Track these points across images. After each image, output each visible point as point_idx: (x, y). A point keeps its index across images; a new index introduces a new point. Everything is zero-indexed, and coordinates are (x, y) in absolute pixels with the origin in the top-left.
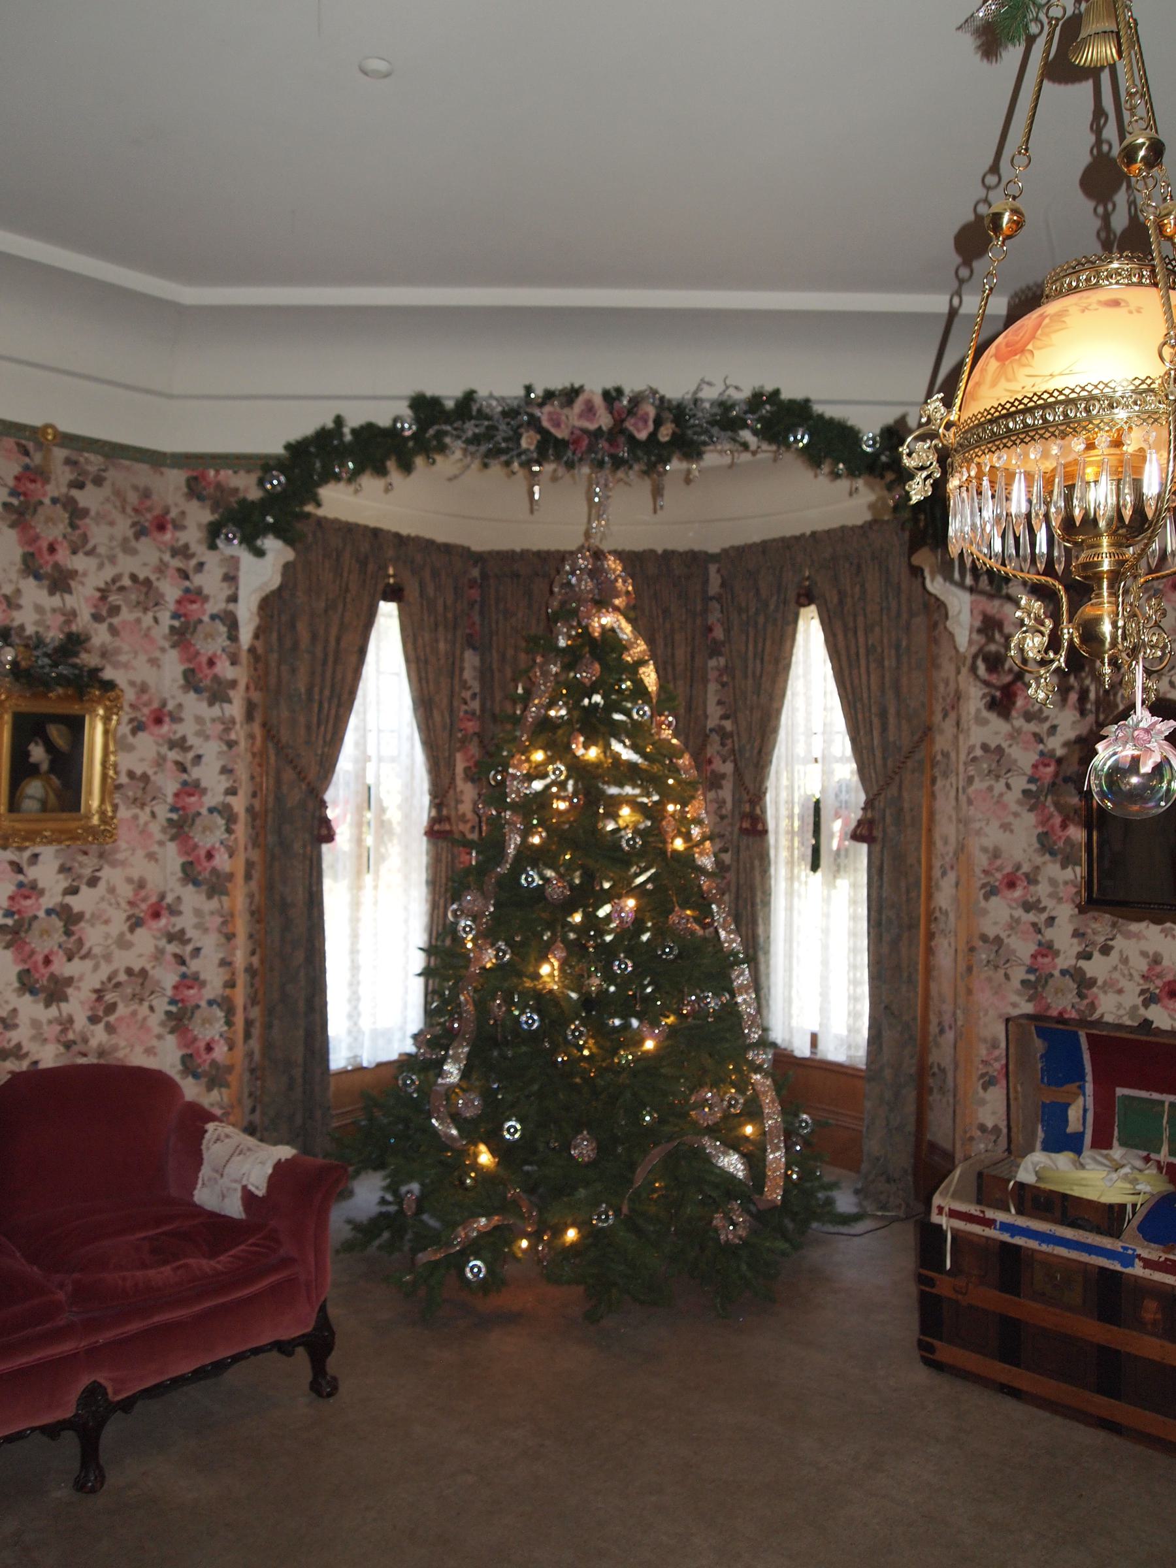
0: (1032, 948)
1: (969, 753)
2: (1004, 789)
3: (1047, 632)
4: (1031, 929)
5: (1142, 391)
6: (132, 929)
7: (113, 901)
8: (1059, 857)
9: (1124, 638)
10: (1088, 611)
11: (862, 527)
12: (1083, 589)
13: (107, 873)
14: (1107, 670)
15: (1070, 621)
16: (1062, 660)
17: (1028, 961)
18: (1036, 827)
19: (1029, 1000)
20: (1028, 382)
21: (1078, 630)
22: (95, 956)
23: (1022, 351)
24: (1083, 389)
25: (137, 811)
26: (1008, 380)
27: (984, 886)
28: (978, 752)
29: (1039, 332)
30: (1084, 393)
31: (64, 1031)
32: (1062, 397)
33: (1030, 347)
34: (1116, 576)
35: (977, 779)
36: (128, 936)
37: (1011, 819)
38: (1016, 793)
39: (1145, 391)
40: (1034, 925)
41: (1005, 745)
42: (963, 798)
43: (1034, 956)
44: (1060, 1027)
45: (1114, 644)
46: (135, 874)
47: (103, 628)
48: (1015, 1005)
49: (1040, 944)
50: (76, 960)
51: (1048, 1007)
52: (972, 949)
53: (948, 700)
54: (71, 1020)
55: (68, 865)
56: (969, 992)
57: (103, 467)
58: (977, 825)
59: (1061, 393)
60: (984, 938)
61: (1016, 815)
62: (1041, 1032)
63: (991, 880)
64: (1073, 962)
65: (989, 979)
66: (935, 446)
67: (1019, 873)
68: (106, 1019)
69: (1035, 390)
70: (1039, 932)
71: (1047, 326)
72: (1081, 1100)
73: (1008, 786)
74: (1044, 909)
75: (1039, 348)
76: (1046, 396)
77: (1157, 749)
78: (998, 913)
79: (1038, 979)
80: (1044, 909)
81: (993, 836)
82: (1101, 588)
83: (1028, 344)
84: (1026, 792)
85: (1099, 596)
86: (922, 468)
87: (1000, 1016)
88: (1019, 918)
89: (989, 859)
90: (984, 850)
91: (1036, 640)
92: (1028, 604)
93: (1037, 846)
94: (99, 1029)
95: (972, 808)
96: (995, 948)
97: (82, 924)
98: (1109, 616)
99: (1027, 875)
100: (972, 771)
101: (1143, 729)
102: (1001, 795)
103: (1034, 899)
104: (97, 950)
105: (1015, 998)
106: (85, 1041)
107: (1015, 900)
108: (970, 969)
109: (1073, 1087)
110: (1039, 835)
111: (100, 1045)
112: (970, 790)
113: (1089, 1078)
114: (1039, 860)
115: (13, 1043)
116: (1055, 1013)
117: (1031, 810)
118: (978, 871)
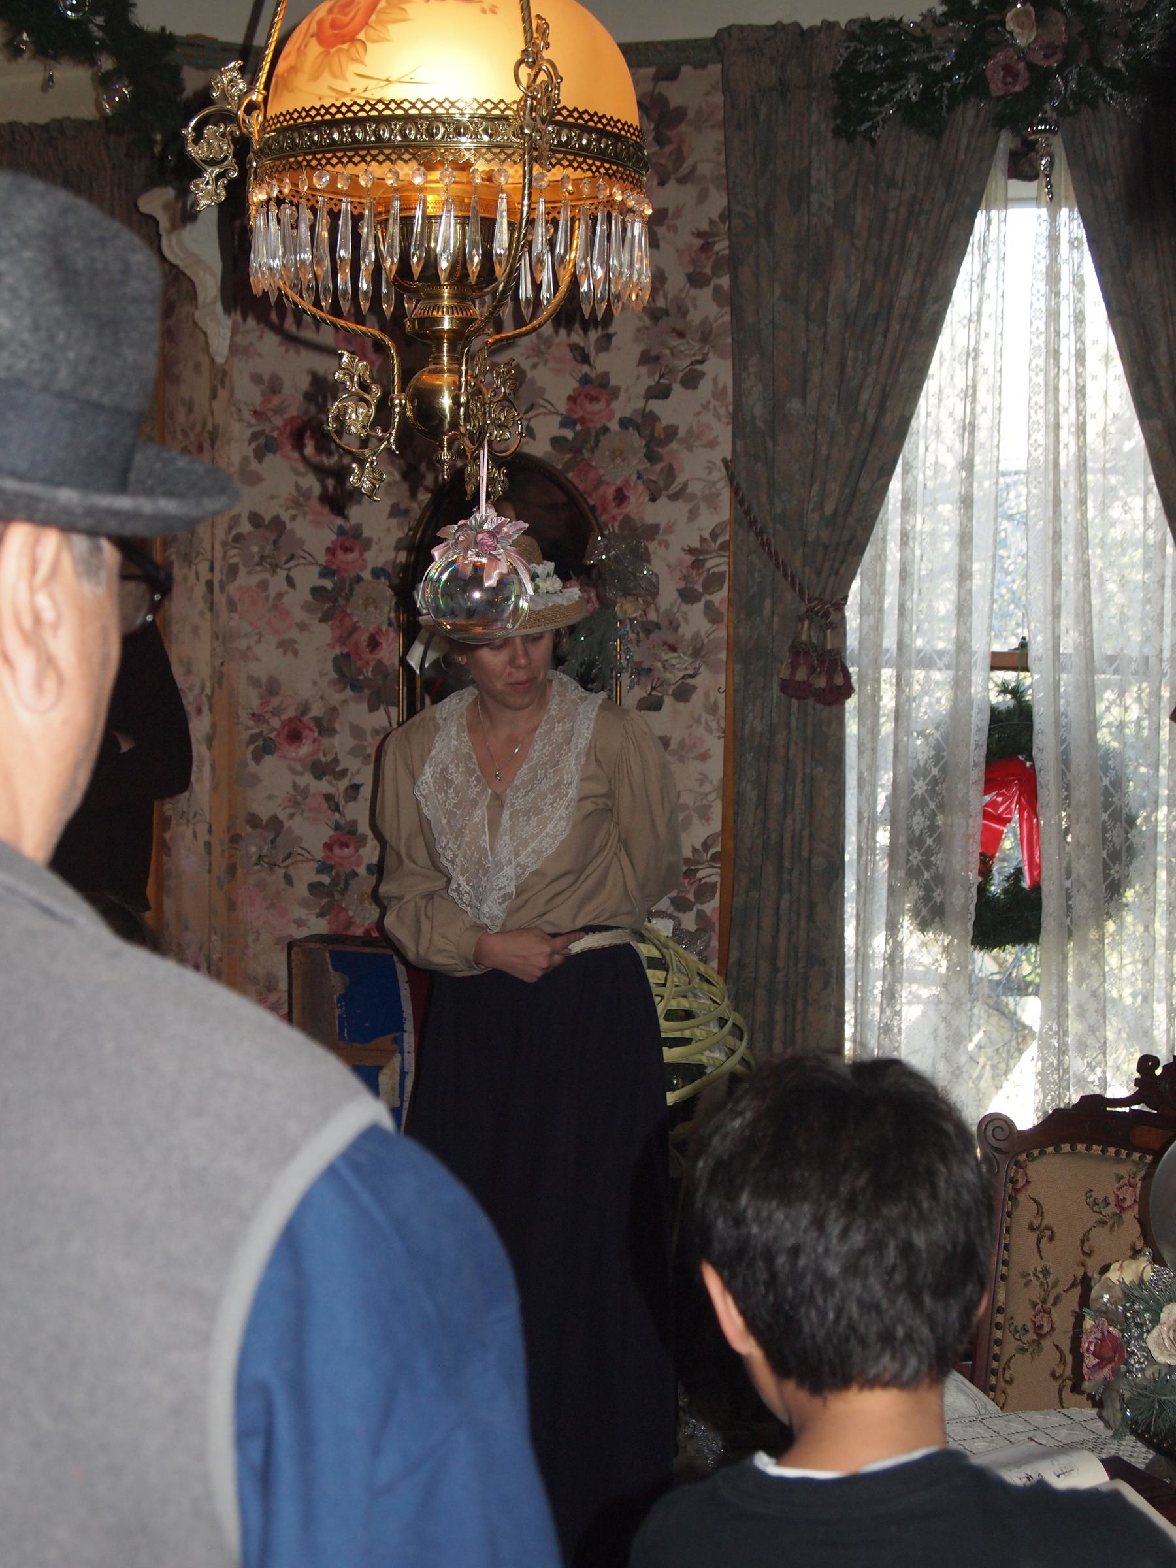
0: (327, 833)
1: (231, 528)
2: (284, 586)
3: (373, 402)
4: (325, 805)
5: (491, 120)
8: (367, 692)
9: (467, 419)
10: (425, 377)
11: (45, 128)
12: (419, 344)
14: (446, 456)
15: (402, 390)
16: (392, 440)
17: (319, 854)
18: (331, 646)
19: (321, 915)
20: (360, 84)
21: (412, 402)
23: (352, 39)
24: (426, 105)
26: (334, 75)
27: (253, 739)
28: (245, 527)
29: (373, 17)
30: (426, 111)
32: (399, 112)
33: (361, 36)
34: (460, 337)
35: (242, 571)
37: (294, 633)
38: (303, 594)
39: (497, 118)
40: (329, 798)
41: (285, 517)
42: (220, 599)
43: (328, 847)
44: (368, 950)
45: (455, 425)
48: (300, 923)
49: (337, 827)
51: (350, 923)
52: (235, 839)
53: (192, 437)
55: (654, 353)
56: (232, 906)
57: (699, 358)
58: (243, 644)
59: (399, 106)
60: (253, 821)
61: (303, 627)
62: (341, 962)
63: (264, 728)
64: (640, 404)
65: (262, 885)
66: (231, 133)
67: (306, 719)
68: (708, 597)
69: (367, 95)
70: (337, 808)
71: (383, 11)
72: (396, 1061)
73: (290, 582)
74: (344, 773)
75: (374, 41)
76: (380, 106)
77: (503, 558)
78: (276, 780)
79: (335, 881)
80: (344, 773)
81: (268, 660)
82: (440, 351)
83: (358, 32)
84: (316, 591)
85: (438, 360)
86: (213, 162)
87: (278, 941)
88: (307, 787)
89: (262, 697)
90: (254, 682)
91: (360, 410)
92: (351, 363)
93: (333, 675)
95: (235, 616)
96: (272, 836)
98: (449, 388)
99: (317, 721)
100: (234, 556)
101: (488, 532)
102: (280, 595)
103: (329, 758)
104: (695, 488)
105: (300, 912)
106: (683, 312)
107: (300, 760)
108: (232, 870)
109: (385, 1041)
110: (336, 660)
111: (696, 636)
112: (231, 588)
113: (409, 1025)
114: (336, 698)
116: (359, 932)
117: (323, 620)
118: (244, 715)
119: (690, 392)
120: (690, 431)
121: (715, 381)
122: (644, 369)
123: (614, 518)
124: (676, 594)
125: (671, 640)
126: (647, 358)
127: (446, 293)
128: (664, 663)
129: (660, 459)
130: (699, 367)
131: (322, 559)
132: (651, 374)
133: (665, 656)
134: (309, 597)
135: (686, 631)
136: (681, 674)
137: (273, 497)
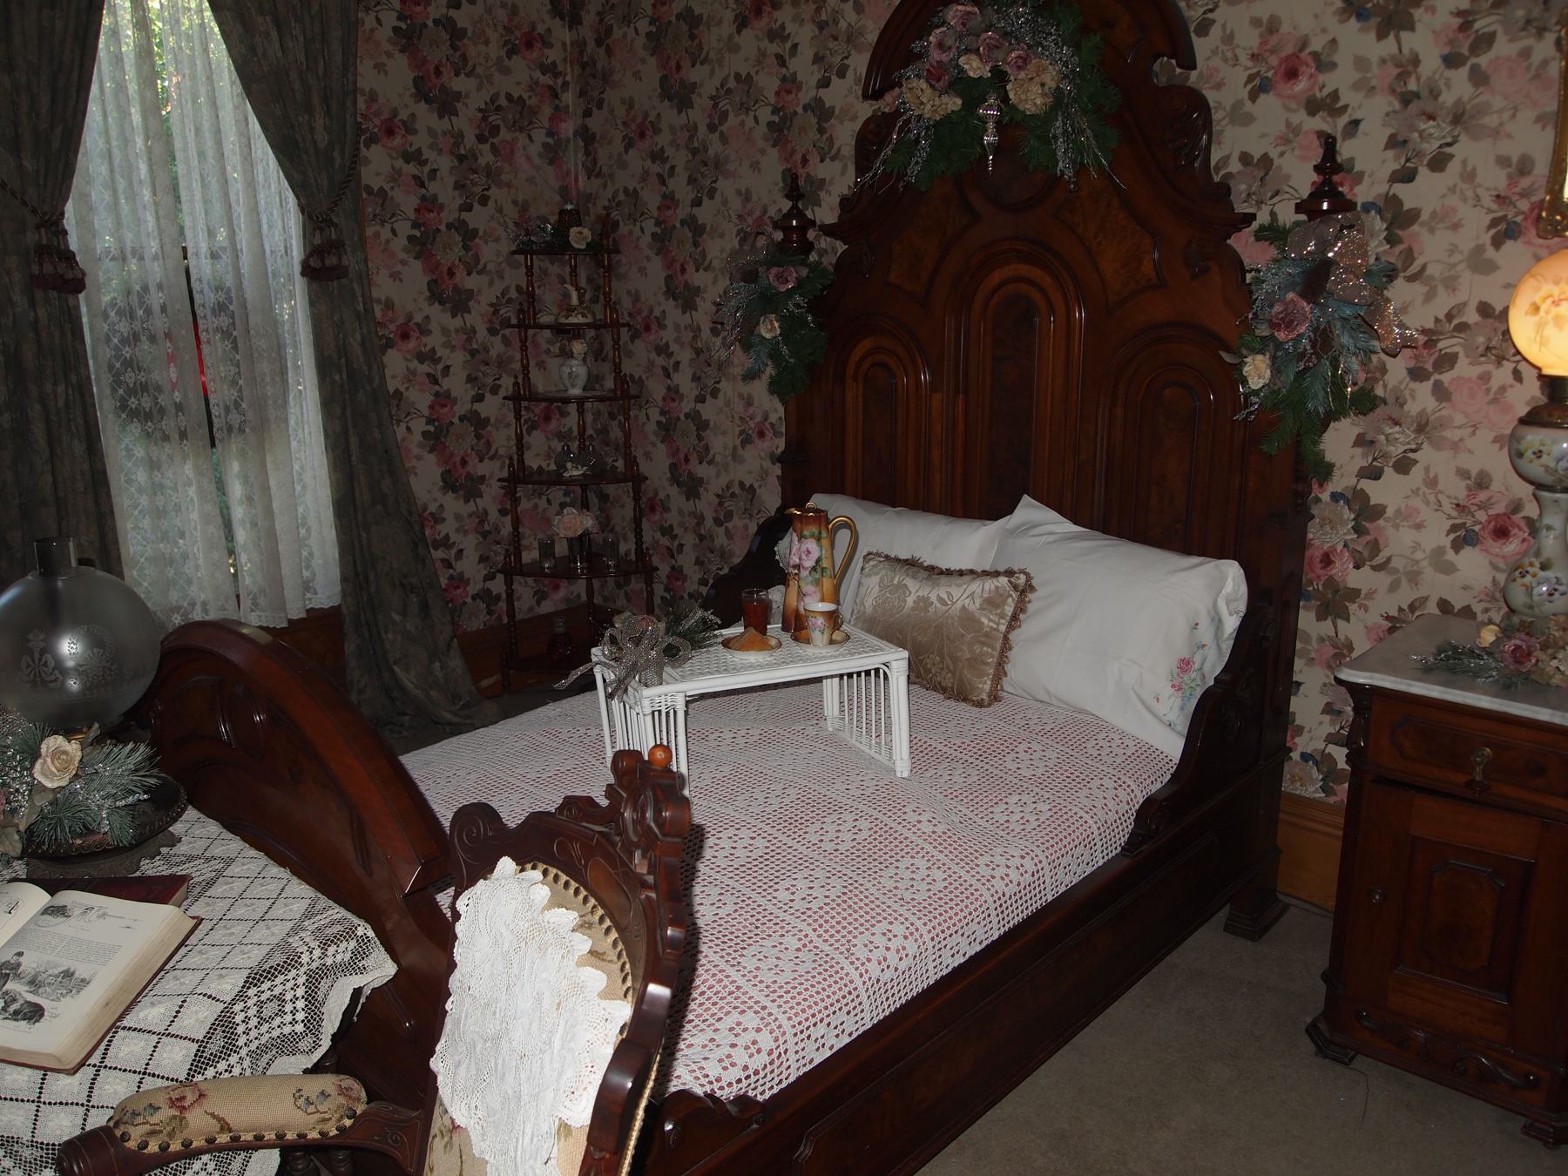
6: (1497, 242)
31: (1403, 76)
36: (1490, 252)
46: (1513, 150)
50: (1366, 569)
54: (1416, 61)
55: (1369, 437)
57: (1449, 140)
68: (1474, 60)
94: (1460, 76)
97: (1415, 228)
104: (1434, 270)
106: (1435, 94)
111: (1459, 102)
115: (1326, 92)
119: (1437, 174)
120: (1434, 214)
122: (1390, 153)
123: (1319, 577)
124: (1439, 61)
125: (1429, 109)
128: (1387, 436)
129: (1400, 241)
130: (1448, 150)
132: (1365, 456)
133: (1422, 126)
135: (1412, 408)
136: (1438, 144)
137: (378, 174)
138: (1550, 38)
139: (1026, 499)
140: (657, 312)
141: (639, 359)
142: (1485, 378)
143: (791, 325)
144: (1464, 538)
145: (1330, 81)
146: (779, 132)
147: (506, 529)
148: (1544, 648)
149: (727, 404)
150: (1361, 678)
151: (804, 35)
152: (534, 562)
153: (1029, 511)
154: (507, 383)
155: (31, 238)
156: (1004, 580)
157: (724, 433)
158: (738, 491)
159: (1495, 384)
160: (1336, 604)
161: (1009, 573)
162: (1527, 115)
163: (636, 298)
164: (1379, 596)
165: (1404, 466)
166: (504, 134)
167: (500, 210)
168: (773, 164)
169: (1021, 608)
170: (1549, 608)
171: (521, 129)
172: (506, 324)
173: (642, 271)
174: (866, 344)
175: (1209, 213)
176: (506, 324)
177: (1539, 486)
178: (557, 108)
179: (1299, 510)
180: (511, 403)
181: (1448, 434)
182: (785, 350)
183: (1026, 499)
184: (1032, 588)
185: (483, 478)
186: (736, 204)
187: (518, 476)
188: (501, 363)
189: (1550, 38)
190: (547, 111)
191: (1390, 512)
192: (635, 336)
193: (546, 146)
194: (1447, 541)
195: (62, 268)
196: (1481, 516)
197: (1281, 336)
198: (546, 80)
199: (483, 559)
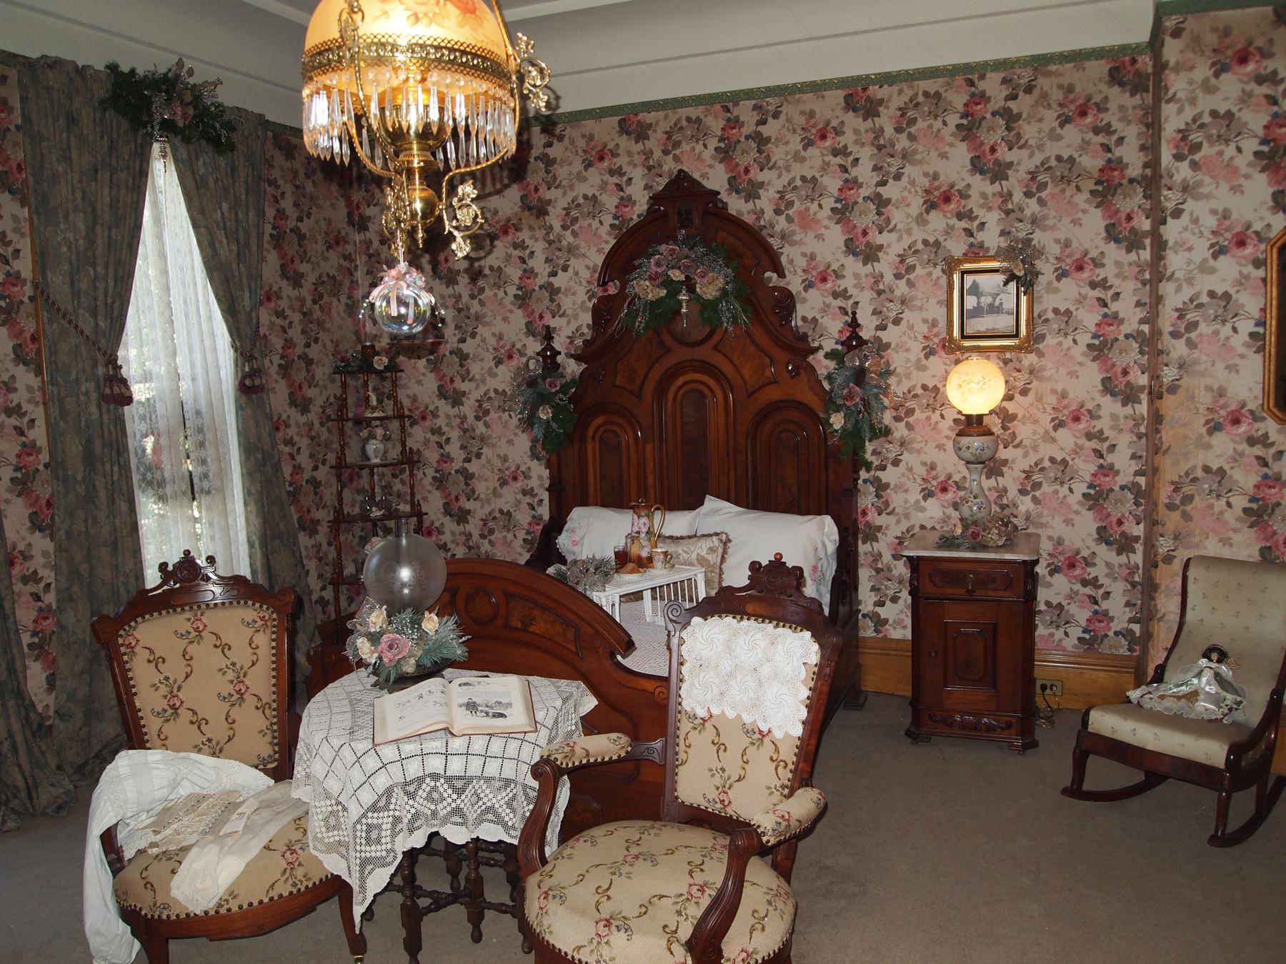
7: (1196, 230)
13: (573, 262)
22: (1026, 446)
25: (1058, 487)
46: (929, 316)
47: (481, 424)
88: (1252, 91)
102: (1069, 349)
107: (1247, 74)
121: (1191, 214)
126: (548, 260)
127: (415, 147)
131: (14, 461)
134: (1247, 339)
138: (939, 268)
139: (708, 497)
140: (284, 417)
141: (417, 437)
142: (928, 418)
143: (557, 409)
144: (928, 494)
145: (843, 284)
146: (523, 299)
147: (333, 554)
148: (984, 530)
149: (489, 461)
150: (912, 554)
151: (539, 247)
152: (352, 575)
153: (711, 503)
154: (331, 458)
155: (101, 371)
156: (715, 538)
157: (486, 480)
158: (498, 515)
159: (933, 421)
160: (872, 534)
161: (717, 534)
162: (933, 301)
163: (415, 399)
164: (892, 528)
165: (896, 463)
166: (326, 299)
167: (324, 346)
168: (519, 318)
169: (725, 552)
170: (980, 515)
171: (334, 295)
172: (329, 418)
173: (419, 382)
174: (599, 420)
175: (800, 347)
176: (329, 418)
177: (968, 462)
178: (352, 282)
179: (853, 492)
180: (333, 471)
181: (914, 445)
182: (555, 425)
183: (708, 497)
184: (730, 541)
185: (318, 521)
186: (492, 342)
187: (340, 520)
188: (327, 445)
189: (939, 268)
190: (347, 283)
191: (892, 486)
192: (414, 423)
193: (347, 305)
194: (920, 497)
195: (124, 390)
196: (934, 483)
197: (848, 404)
198: (346, 264)
199: (320, 576)
